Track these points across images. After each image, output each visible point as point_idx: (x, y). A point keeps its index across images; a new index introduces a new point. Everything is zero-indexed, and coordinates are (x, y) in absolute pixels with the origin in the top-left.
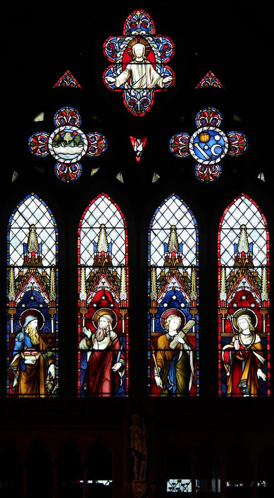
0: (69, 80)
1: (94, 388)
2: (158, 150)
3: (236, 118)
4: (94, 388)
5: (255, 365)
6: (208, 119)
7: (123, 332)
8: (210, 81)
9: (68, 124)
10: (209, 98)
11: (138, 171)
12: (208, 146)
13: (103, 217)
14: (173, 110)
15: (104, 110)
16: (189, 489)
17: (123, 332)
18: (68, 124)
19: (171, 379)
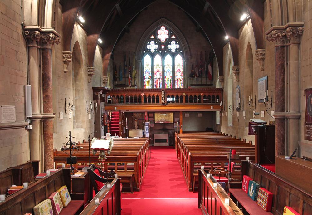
0: (152, 37)
1: (146, 39)
2: (166, 48)
3: (177, 42)
4: (146, 39)
5: (180, 80)
6: (173, 42)
7: (126, 118)
8: (173, 37)
9: (152, 43)
10: (173, 39)
11: (163, 51)
12: (173, 46)
13: (158, 58)
14: (168, 41)
15: (158, 42)
16: (237, 163)
17: (126, 118)
18: (152, 43)
19: (168, 83)
